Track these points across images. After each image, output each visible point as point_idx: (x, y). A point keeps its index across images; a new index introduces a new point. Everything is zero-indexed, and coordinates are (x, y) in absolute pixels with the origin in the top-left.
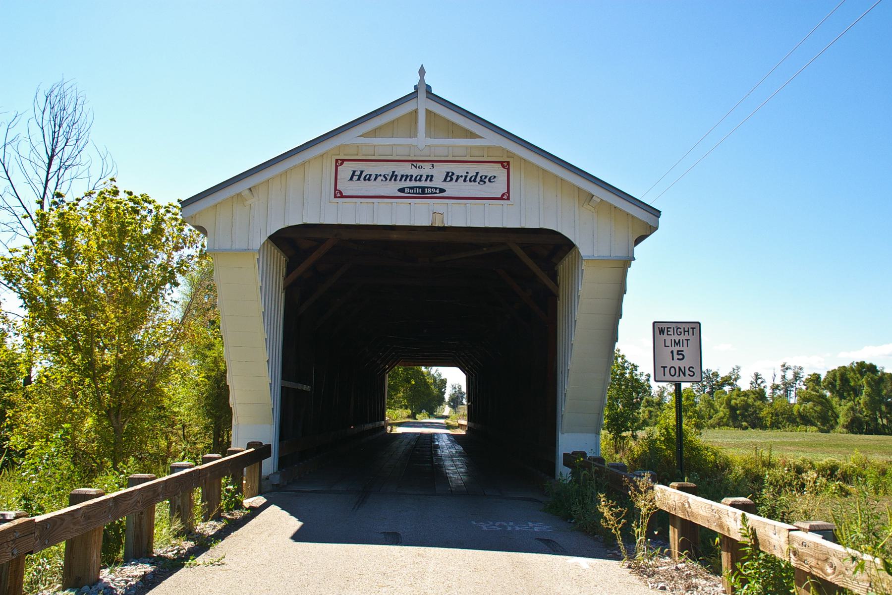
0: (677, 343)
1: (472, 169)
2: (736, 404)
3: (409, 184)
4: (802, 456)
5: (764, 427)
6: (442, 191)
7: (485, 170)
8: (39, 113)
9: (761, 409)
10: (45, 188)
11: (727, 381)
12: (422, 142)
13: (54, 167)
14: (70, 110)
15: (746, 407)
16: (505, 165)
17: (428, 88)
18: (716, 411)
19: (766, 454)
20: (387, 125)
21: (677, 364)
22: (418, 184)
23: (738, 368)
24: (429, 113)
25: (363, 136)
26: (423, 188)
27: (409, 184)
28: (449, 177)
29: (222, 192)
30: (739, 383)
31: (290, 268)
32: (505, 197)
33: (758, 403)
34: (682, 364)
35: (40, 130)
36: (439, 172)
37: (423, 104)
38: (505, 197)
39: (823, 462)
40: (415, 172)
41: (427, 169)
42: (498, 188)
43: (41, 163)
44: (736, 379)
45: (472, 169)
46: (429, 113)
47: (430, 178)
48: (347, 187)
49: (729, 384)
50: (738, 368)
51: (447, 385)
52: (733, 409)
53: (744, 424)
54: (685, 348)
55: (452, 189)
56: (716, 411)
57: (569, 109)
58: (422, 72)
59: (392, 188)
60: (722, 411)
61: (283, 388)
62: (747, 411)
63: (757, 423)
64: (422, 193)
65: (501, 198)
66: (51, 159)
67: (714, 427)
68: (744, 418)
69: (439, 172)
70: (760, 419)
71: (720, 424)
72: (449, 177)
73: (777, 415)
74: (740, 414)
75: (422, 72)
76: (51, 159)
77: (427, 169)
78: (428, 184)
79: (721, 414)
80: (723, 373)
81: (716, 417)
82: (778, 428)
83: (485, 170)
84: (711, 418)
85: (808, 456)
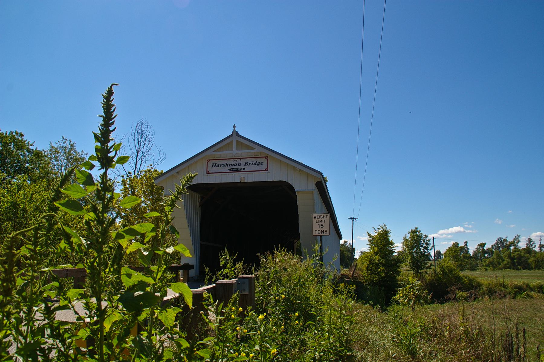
0: (321, 221)
1: (255, 160)
2: (514, 256)
3: (232, 167)
4: (523, 281)
5: (530, 269)
6: (244, 169)
7: (259, 160)
8: (133, 133)
9: (529, 259)
10: (136, 165)
11: (512, 244)
12: (234, 152)
13: (139, 157)
14: (144, 132)
15: (520, 257)
16: (267, 158)
17: (237, 132)
18: (503, 260)
19: (501, 280)
20: (226, 145)
21: (321, 229)
22: (235, 167)
23: (518, 236)
24: (237, 141)
25: (215, 151)
26: (237, 168)
27: (232, 167)
28: (246, 163)
29: (173, 171)
30: (519, 244)
31: (202, 198)
32: (267, 170)
33: (527, 255)
34: (322, 229)
35: (133, 141)
36: (243, 162)
37: (235, 138)
38: (267, 170)
39: (535, 284)
40: (234, 163)
41: (239, 161)
42: (264, 167)
43: (133, 155)
44: (518, 243)
45: (255, 160)
46: (237, 141)
47: (240, 164)
48: (211, 170)
49: (513, 245)
50: (518, 236)
51: (356, 251)
52: (512, 259)
53: (519, 267)
54: (323, 223)
55: (247, 168)
56: (503, 260)
57: (293, 137)
58: (234, 127)
59: (226, 169)
60: (507, 260)
61: (201, 245)
62: (520, 260)
63: (527, 266)
64: (237, 170)
65: (265, 170)
66: (138, 153)
67: (502, 269)
68: (519, 265)
69: (243, 162)
70: (529, 264)
71: (506, 267)
72: (246, 163)
73: (538, 262)
74: (517, 262)
75: (234, 127)
76: (138, 153)
77: (239, 161)
78: (239, 167)
79: (505, 262)
80: (510, 239)
81: (503, 264)
82: (539, 269)
83: (259, 160)
84: (500, 264)
85: (526, 281)
